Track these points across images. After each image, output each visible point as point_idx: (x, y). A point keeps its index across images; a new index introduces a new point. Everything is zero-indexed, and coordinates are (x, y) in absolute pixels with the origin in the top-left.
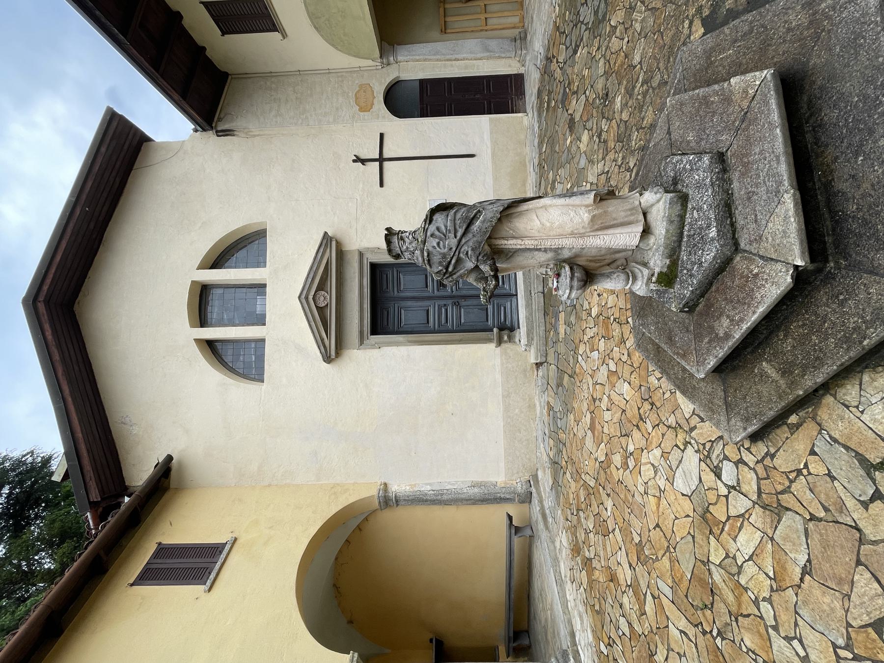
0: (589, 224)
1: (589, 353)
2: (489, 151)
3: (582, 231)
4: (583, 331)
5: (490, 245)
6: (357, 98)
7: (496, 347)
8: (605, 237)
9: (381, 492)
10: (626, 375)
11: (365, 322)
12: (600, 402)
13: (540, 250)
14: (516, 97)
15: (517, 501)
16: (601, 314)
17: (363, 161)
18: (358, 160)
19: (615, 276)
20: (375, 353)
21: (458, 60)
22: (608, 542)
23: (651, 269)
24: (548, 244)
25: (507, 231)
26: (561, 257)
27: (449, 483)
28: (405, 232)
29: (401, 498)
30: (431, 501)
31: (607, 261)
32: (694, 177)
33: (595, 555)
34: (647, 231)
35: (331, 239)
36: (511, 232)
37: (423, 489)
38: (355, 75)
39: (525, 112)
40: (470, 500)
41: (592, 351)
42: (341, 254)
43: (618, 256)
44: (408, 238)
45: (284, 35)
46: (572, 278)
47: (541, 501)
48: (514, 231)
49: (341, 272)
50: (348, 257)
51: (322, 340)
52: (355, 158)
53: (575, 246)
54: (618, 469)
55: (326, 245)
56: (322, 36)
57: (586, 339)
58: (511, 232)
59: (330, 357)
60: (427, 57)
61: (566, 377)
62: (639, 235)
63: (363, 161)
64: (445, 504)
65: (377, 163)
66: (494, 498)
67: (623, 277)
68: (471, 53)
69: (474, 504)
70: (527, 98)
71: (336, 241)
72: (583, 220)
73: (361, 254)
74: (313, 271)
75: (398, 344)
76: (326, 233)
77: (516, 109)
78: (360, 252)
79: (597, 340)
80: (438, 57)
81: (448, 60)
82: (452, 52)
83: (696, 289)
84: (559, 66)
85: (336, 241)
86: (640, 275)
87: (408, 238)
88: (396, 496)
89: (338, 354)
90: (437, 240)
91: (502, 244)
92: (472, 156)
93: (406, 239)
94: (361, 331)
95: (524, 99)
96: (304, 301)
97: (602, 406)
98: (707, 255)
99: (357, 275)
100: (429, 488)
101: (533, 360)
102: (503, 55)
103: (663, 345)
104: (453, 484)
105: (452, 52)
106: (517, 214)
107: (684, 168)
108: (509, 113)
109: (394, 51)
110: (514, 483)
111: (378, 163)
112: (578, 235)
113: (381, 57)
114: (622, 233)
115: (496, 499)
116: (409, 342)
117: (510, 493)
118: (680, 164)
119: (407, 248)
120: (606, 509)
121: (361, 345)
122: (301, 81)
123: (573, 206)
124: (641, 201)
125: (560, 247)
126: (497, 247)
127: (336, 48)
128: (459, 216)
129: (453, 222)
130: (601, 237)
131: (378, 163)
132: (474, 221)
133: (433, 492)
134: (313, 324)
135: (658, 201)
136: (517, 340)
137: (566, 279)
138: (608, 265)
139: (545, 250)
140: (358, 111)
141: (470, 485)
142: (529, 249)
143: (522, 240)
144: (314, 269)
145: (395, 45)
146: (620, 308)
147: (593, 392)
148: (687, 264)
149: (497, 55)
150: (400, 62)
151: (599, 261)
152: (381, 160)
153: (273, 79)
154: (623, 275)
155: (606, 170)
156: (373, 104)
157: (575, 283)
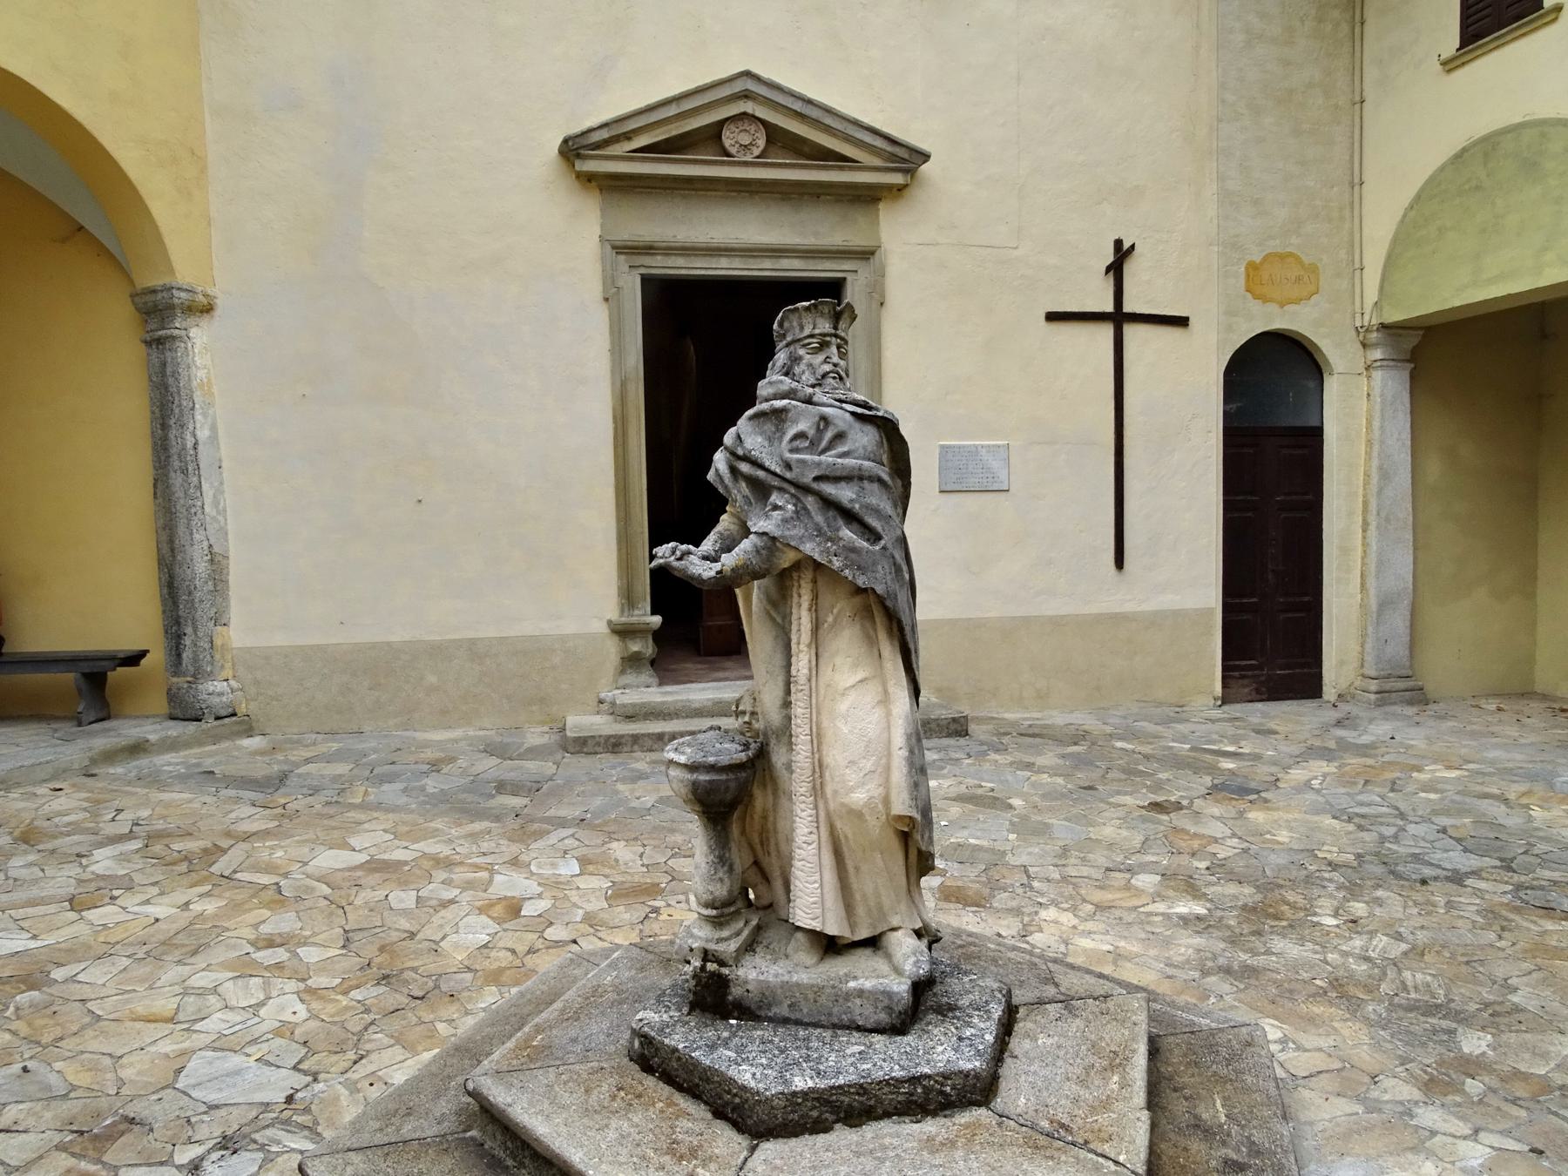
0: (843, 805)
2: (1129, 607)
3: (829, 790)
5: (797, 566)
6: (1282, 257)
7: (610, 622)
9: (183, 295)
10: (508, 940)
11: (680, 262)
12: (443, 883)
13: (788, 692)
14: (1263, 678)
15: (175, 680)
17: (1116, 269)
18: (1122, 254)
20: (593, 287)
21: (1364, 531)
22: (52, 908)
24: (799, 709)
25: (833, 607)
26: (773, 742)
27: (219, 492)
29: (168, 354)
30: (165, 438)
31: (765, 861)
32: (942, 1045)
33: (15, 880)
34: (830, 946)
35: (911, 172)
36: (830, 619)
37: (198, 417)
38: (1343, 254)
39: (1226, 700)
40: (172, 550)
41: (584, 862)
42: (867, 197)
43: (778, 884)
44: (825, 361)
45: (1450, 65)
46: (712, 768)
47: (172, 745)
48: (832, 626)
49: (802, 194)
50: (860, 217)
51: (628, 136)
52: (1126, 245)
54: (256, 926)
55: (893, 157)
56: (1442, 169)
58: (830, 619)
59: (578, 156)
60: (1376, 448)
62: (816, 925)
63: (1116, 269)
64: (156, 480)
65: (1109, 307)
66: (179, 617)
68: (1380, 563)
69: (161, 561)
70: (1259, 705)
71: (906, 186)
72: (852, 790)
73: (866, 255)
74: (809, 112)
75: (617, 350)
76: (925, 157)
78: (873, 253)
79: (607, 871)
80: (1375, 480)
81: (1365, 504)
82: (1383, 515)
83: (679, 1059)
84: (1316, 778)
85: (906, 186)
86: (725, 933)
87: (825, 361)
88: (174, 338)
89: (588, 179)
91: (800, 596)
92: (1119, 562)
93: (821, 357)
94: (651, 248)
95: (1259, 697)
96: (738, 87)
97: (431, 887)
98: (754, 1074)
99: (809, 241)
100: (203, 434)
102: (1368, 646)
104: (216, 503)
105: (1383, 515)
106: (872, 632)
109: (1394, 361)
110: (228, 673)
111: (1124, 311)
113: (1384, 327)
114: (821, 885)
115: (178, 623)
116: (623, 384)
117: (195, 660)
119: (800, 358)
120: (147, 902)
121: (614, 247)
122: (1336, 107)
123: (888, 768)
125: (793, 739)
126: (796, 584)
127: (1411, 207)
130: (814, 837)
131: (1124, 311)
132: (855, 526)
133: (190, 444)
134: (672, 111)
136: (629, 678)
138: (756, 863)
139: (787, 704)
140: (1249, 258)
141: (216, 549)
142: (789, 665)
144: (828, 121)
145: (1412, 365)
148: (742, 1038)
149: (1370, 629)
150: (1369, 377)
151: (764, 842)
152: (1119, 318)
153: (1345, 28)
154: (725, 893)
155: (1036, 884)
156: (1264, 299)
157: (703, 777)
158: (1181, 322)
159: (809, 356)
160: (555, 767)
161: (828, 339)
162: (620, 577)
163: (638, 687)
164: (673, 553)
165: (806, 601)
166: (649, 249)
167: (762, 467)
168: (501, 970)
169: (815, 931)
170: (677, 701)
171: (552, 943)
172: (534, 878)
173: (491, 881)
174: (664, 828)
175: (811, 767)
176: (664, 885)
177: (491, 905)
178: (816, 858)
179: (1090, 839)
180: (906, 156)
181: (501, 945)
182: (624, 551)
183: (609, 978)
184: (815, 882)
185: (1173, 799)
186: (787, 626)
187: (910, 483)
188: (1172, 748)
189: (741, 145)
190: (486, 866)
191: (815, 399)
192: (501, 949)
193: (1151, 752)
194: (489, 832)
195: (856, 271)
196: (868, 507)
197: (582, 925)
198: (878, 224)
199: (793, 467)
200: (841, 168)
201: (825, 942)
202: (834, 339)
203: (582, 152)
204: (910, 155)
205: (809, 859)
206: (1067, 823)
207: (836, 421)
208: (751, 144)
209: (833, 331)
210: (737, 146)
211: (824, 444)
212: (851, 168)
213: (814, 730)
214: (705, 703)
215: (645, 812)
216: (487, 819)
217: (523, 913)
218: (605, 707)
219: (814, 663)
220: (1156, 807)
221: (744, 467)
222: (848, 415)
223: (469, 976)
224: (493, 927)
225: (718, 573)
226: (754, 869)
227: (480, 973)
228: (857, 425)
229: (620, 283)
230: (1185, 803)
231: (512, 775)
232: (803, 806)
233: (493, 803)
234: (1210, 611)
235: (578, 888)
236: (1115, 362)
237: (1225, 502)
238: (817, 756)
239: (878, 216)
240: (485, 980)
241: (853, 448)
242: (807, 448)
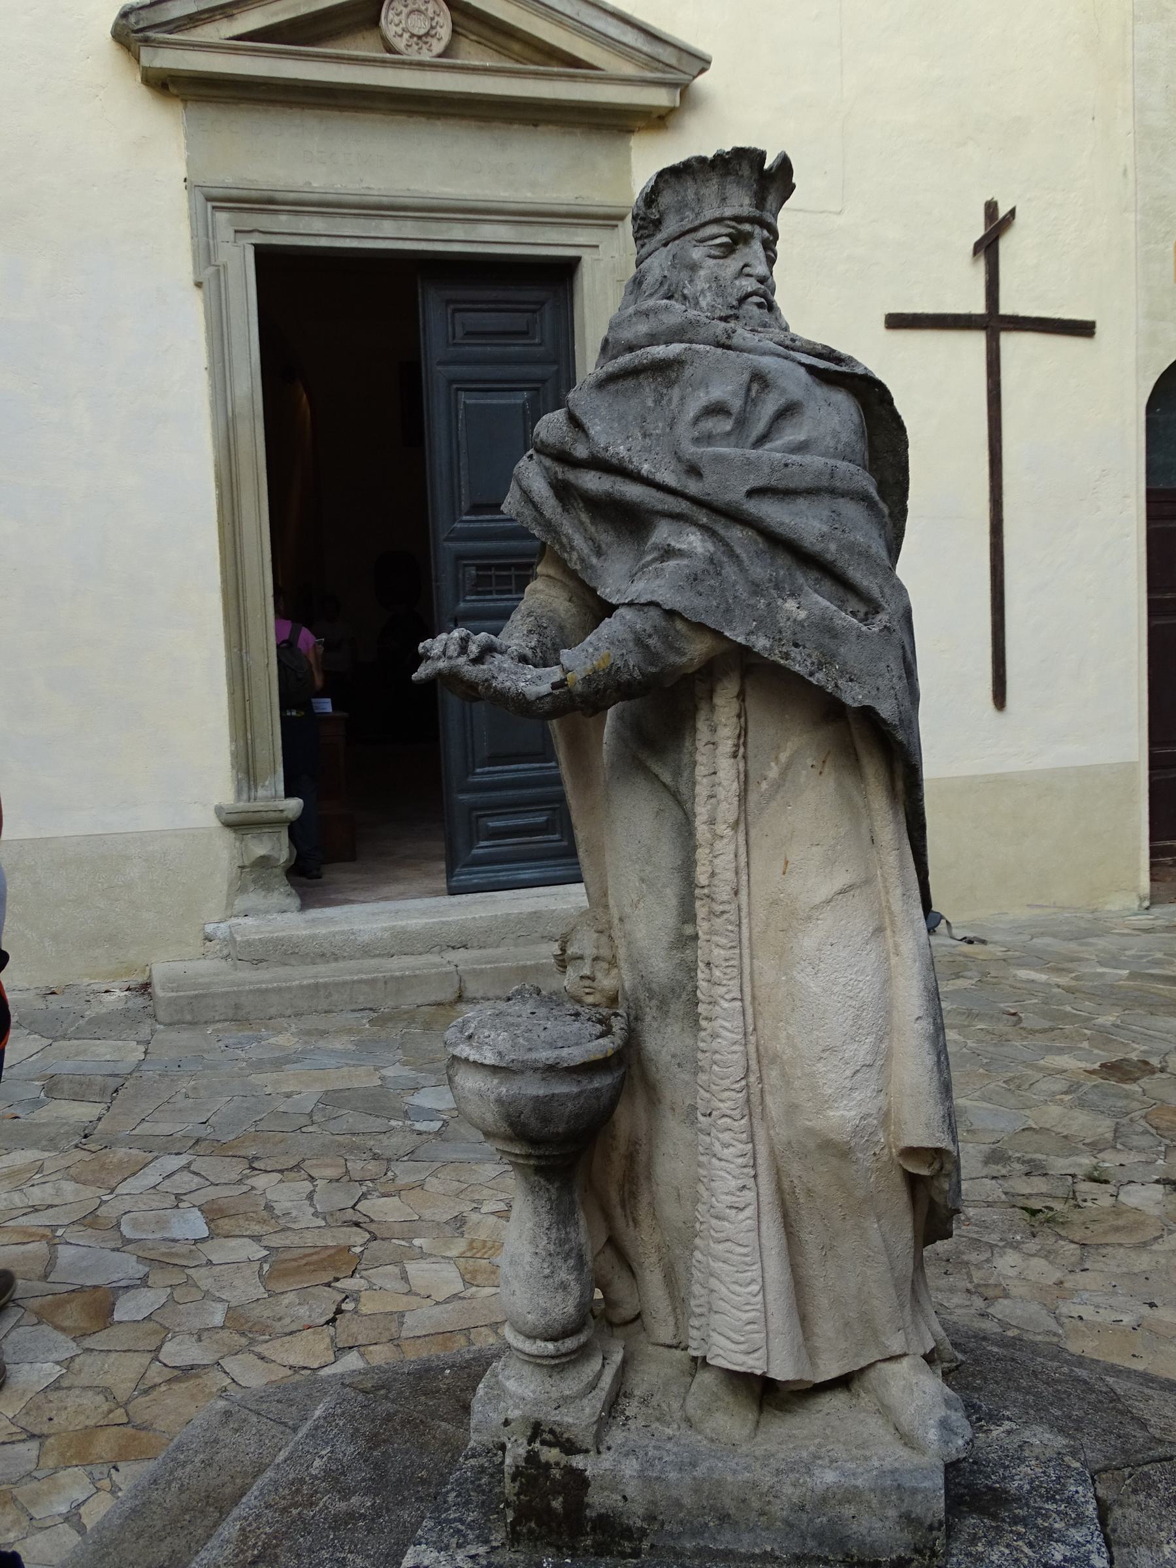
0: (810, 1132)
1: (200, 1198)
2: (1016, 765)
4: (297, 1167)
7: (219, 810)
8: (750, 1211)
11: (318, 225)
13: (687, 915)
16: (374, 1238)
19: (563, 1275)
23: (598, 1438)
25: (778, 748)
26: (650, 1013)
28: (771, 261)
41: (213, 1213)
43: (653, 1279)
46: (552, 1070)
48: (778, 786)
52: (1003, 212)
53: (703, 1077)
57: (261, 1181)
58: (773, 772)
59: (147, 41)
61: (83, 1112)
62: (754, 1364)
67: (564, 1307)
71: (672, 110)
77: (1164, 864)
79: (257, 1229)
86: (571, 1384)
87: (741, 273)
90: (736, 404)
91: (714, 730)
93: (732, 265)
101: (161, 970)
103: (230, 1529)
107: (1049, 1535)
108: (1153, 838)
112: (755, 1089)
114: (763, 1288)
118: (1063, 1515)
119: (693, 267)
121: (209, 199)
124: (905, 1362)
125: (701, 1008)
128: (852, 511)
129: (825, 482)
130: (750, 1195)
132: (827, 585)
135: (907, 1440)
136: (254, 898)
137: (553, 1045)
139: (685, 941)
143: (735, 826)
146: (402, 1315)
147: (14, 1230)
154: (571, 1309)
157: (534, 1088)
158: (1084, 329)
159: (712, 262)
160: (142, 1048)
161: (747, 227)
162: (234, 739)
163: (267, 912)
164: (463, 649)
165: (726, 735)
166: (266, 203)
167: (635, 477)
168: (89, 1433)
169: (752, 1374)
170: (334, 934)
171: (176, 1373)
172: (130, 1247)
173: (52, 1261)
174: (340, 1145)
175: (743, 1062)
176: (358, 1250)
177: (59, 1305)
178: (754, 1234)
179: (1029, 1129)
180: (673, 61)
181: (83, 1381)
182: (238, 694)
183: (317, 1463)
184: (753, 1281)
185: (1134, 1056)
186: (683, 789)
187: (904, 512)
188: (1102, 975)
189: (412, 36)
190: (42, 1231)
191: (736, 340)
192: (86, 1388)
193: (1073, 983)
194: (40, 1170)
195: (597, 247)
196: (851, 548)
197: (225, 1334)
198: (629, 172)
199: (706, 471)
200: (572, 77)
201: (758, 1389)
202: (757, 230)
203: (151, 34)
204: (679, 60)
205: (742, 1238)
206: (985, 1105)
207: (783, 382)
208: (427, 34)
209: (757, 213)
210: (406, 36)
211: (759, 427)
212: (586, 78)
213: (747, 990)
214: (379, 934)
215: (304, 1120)
216: (35, 1145)
217: (117, 1317)
218: (214, 946)
219: (743, 859)
220: (1117, 1070)
221: (592, 482)
222: (802, 370)
223: (30, 1449)
224: (67, 1347)
225: (555, 686)
226: (609, 1253)
227: (51, 1440)
228: (821, 392)
229: (221, 259)
230: (1155, 1061)
231: (68, 1066)
232: (726, 1137)
233: (42, 1115)
234: (1132, 766)
235: (210, 1263)
236: (990, 391)
237: (1150, 603)
238: (752, 1039)
239: (628, 161)
240: (62, 1455)
241: (815, 434)
242: (729, 434)
